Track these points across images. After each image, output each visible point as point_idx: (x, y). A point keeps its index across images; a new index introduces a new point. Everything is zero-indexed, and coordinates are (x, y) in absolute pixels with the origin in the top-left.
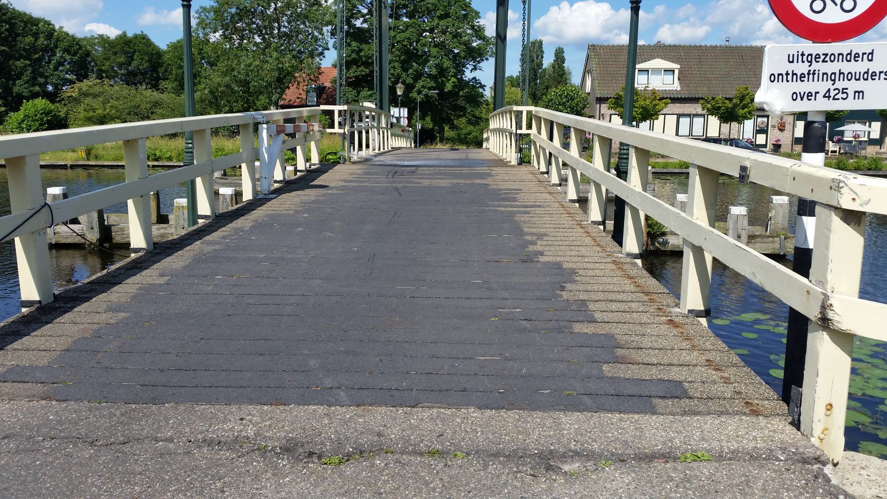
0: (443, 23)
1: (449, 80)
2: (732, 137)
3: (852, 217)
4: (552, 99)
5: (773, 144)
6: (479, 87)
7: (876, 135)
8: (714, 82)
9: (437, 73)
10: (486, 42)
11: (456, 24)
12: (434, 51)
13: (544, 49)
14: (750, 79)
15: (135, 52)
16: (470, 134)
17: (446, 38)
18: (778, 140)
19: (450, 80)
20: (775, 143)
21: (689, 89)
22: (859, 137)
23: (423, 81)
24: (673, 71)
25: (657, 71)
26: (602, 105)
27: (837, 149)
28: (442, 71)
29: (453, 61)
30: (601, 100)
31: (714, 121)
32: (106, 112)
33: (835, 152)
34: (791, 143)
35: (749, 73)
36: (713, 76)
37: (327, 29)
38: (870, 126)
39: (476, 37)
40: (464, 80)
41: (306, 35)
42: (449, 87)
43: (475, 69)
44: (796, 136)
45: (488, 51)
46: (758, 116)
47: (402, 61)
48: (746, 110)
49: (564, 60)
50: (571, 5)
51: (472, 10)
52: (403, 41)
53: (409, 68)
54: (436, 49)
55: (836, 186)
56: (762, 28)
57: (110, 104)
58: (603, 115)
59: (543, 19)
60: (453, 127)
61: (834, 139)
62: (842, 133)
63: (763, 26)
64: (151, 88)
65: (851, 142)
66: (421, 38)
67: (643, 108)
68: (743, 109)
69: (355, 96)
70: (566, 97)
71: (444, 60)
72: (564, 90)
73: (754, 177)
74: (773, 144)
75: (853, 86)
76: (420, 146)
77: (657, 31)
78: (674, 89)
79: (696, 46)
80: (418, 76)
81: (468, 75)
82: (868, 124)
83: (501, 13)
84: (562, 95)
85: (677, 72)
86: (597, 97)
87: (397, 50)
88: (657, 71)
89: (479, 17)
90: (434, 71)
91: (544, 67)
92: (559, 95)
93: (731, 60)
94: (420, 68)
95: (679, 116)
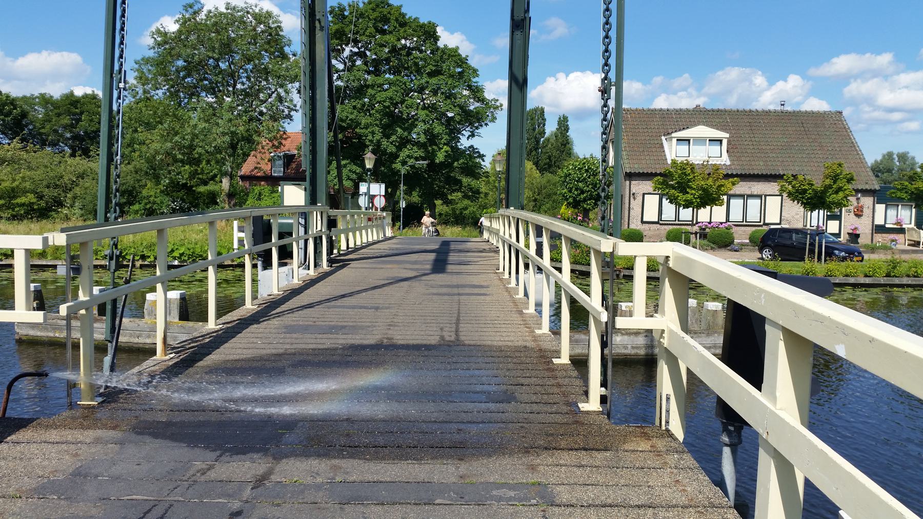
0: (434, 81)
1: (440, 149)
4: (570, 174)
5: (848, 233)
6: (477, 157)
8: (771, 155)
9: (425, 140)
10: (486, 105)
11: (449, 83)
12: (422, 114)
13: (546, 116)
14: (816, 152)
15: (82, 113)
16: (466, 209)
17: (437, 100)
18: (856, 229)
19: (442, 149)
20: (851, 231)
21: (741, 163)
23: (409, 150)
24: (721, 141)
25: (700, 141)
26: (633, 182)
28: (432, 139)
29: (446, 126)
30: (630, 176)
32: (14, 185)
34: (871, 231)
36: (768, 147)
37: (294, 87)
39: (474, 99)
40: (459, 149)
41: (269, 94)
42: (440, 157)
43: (473, 135)
44: (876, 223)
45: (488, 116)
47: (385, 125)
49: (568, 129)
50: (567, 76)
51: (469, 67)
52: (384, 101)
53: (392, 134)
54: (425, 111)
56: (760, 99)
57: (21, 175)
58: (634, 194)
59: (539, 88)
60: (447, 202)
63: (760, 97)
64: (80, 156)
66: (407, 98)
67: (704, 190)
68: (837, 192)
70: (587, 171)
71: (435, 125)
72: (584, 163)
74: (848, 233)
76: (403, 228)
77: (653, 101)
78: (722, 163)
79: (745, 111)
80: (403, 143)
81: (464, 142)
83: (519, 42)
84: (582, 168)
85: (725, 142)
86: (626, 173)
87: (377, 111)
88: (700, 141)
89: (477, 76)
90: (423, 139)
91: (546, 135)
92: (579, 169)
93: (790, 129)
94: (406, 134)
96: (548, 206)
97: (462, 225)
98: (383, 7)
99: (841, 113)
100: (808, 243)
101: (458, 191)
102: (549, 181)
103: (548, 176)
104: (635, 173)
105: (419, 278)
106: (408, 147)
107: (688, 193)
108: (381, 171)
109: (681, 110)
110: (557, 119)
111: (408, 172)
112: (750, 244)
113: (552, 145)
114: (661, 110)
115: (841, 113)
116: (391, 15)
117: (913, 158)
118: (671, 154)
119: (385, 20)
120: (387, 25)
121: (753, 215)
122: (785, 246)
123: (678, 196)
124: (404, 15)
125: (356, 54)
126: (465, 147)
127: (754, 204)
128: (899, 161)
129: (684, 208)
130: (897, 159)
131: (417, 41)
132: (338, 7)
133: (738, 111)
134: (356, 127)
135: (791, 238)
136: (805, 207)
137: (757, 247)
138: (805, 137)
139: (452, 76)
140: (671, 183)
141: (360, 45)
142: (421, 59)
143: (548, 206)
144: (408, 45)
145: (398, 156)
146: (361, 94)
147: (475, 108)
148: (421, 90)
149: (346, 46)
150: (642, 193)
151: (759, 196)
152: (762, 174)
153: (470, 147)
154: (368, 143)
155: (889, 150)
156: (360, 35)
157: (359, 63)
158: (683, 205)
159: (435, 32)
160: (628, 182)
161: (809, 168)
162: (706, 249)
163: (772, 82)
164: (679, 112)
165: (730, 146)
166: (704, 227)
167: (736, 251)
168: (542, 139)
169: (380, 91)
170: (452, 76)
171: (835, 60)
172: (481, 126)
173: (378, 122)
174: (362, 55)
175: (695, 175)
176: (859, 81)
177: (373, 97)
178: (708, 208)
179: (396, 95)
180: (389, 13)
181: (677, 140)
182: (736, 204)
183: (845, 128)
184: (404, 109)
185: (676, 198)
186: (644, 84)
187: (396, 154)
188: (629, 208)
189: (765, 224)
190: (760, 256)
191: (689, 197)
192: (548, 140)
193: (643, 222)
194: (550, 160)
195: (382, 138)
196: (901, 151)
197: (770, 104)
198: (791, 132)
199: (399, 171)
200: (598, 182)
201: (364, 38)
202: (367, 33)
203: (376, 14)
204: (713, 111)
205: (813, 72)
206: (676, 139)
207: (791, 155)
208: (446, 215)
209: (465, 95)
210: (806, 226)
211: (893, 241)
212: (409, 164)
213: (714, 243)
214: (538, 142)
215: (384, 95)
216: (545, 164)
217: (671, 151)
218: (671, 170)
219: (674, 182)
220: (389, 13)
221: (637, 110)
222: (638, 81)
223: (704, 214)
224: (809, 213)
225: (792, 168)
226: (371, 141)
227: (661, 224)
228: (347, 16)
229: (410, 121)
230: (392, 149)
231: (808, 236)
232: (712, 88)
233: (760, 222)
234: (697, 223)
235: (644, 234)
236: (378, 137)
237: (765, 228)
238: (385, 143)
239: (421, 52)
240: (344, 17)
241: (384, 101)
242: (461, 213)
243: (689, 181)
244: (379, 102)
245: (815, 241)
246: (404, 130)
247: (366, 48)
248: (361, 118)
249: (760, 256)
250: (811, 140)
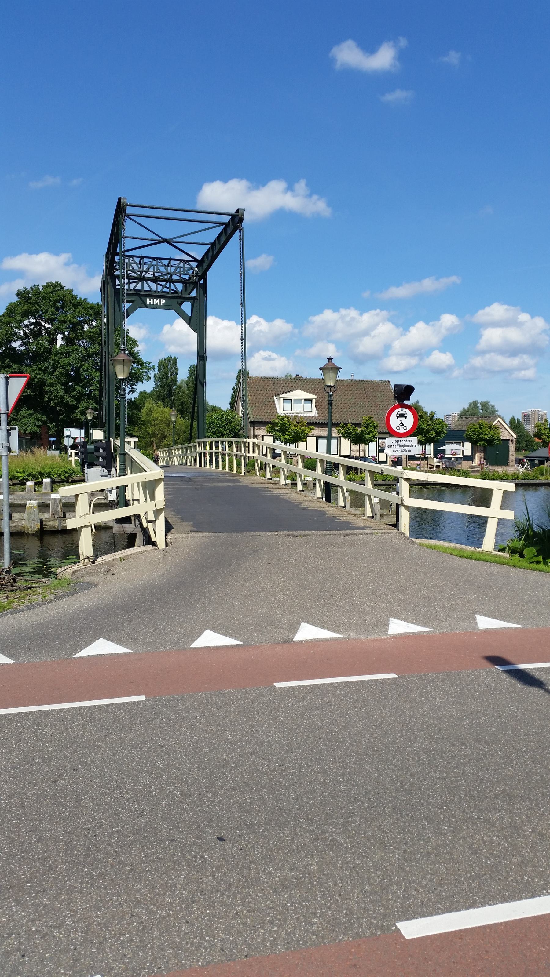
2: (361, 456)
3: (406, 480)
7: (468, 453)
14: (372, 408)
20: (393, 460)
22: (456, 454)
25: (298, 400)
26: (256, 428)
27: (440, 464)
30: (254, 424)
31: (345, 443)
33: (439, 466)
35: (370, 403)
38: (463, 446)
46: (379, 438)
48: (371, 435)
55: (402, 473)
58: (256, 436)
61: (438, 457)
62: (443, 451)
65: (450, 458)
67: (295, 433)
69: (14, 415)
72: (222, 415)
73: (385, 472)
75: (408, 448)
82: (462, 444)
85: (314, 401)
91: (178, 383)
93: (356, 392)
95: (318, 438)
99: (389, 381)
110: (188, 369)
114: (273, 378)
115: (389, 381)
117: (493, 406)
124: (75, 297)
128: (482, 409)
130: (480, 407)
132: (24, 291)
155: (475, 400)
165: (318, 404)
187: (76, 406)
191: (287, 436)
194: (183, 407)
196: (484, 400)
198: (357, 395)
207: (356, 410)
211: (418, 465)
217: (280, 407)
221: (257, 377)
230: (73, 402)
236: (61, 393)
238: (67, 397)
240: (30, 298)
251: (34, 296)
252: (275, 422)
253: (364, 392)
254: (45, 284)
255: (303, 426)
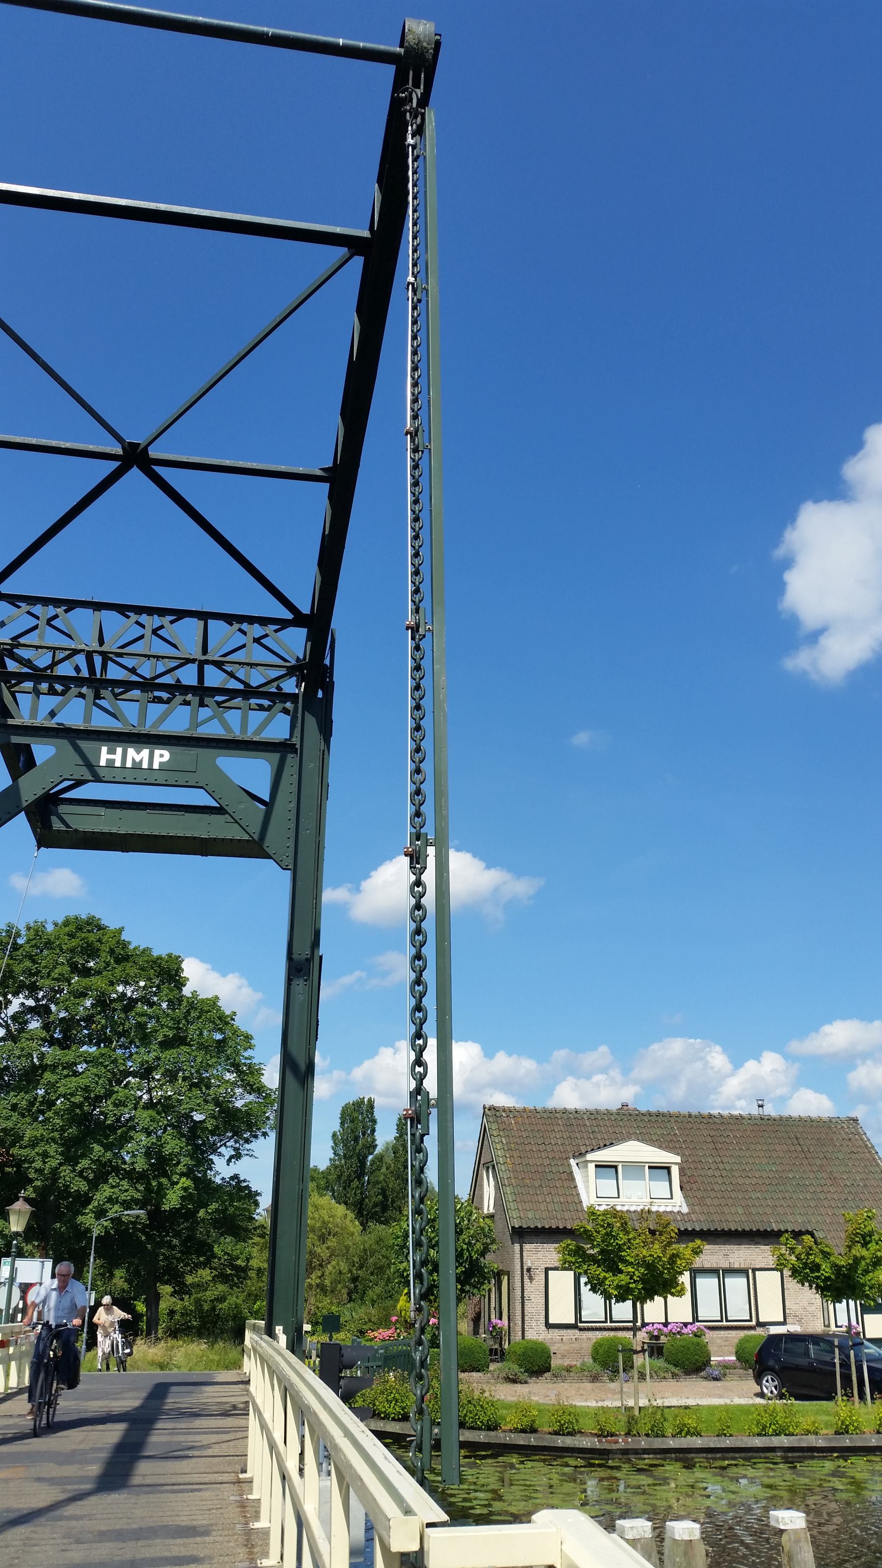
0: (169, 1055)
8: (754, 1195)
10: (265, 1098)
12: (144, 1117)
13: (377, 1114)
14: (825, 1189)
16: (221, 1299)
19: (177, 1183)
25: (634, 1168)
26: (527, 1247)
30: (522, 1234)
35: (819, 1175)
36: (747, 1181)
42: (172, 1199)
43: (237, 1156)
47: (70, 1139)
52: (72, 1095)
53: (83, 1156)
60: (181, 1290)
67: (650, 1266)
78: (676, 1210)
85: (675, 1171)
86: (513, 1228)
90: (141, 1164)
93: (778, 1147)
94: (109, 1155)
96: (378, 1290)
97: (208, 1337)
98: (89, 931)
100: (837, 1361)
101: (205, 1267)
102: (379, 1241)
103: (378, 1229)
104: (529, 1228)
105: (58, 1513)
106: (111, 1181)
107: (621, 1272)
108: (55, 1229)
109: (598, 1112)
111: (107, 1232)
112: (738, 1364)
113: (387, 1169)
114: (565, 1111)
116: (102, 943)
118: (588, 1192)
119: (91, 951)
120: (93, 960)
121: (738, 1310)
122: (797, 1368)
123: (605, 1278)
124: (125, 945)
125: (31, 1010)
126: (223, 1179)
127: (736, 1285)
129: (617, 1301)
131: (144, 988)
133: (690, 1116)
134: (13, 1145)
135: (807, 1353)
136: (823, 1296)
137: (751, 1371)
138: (805, 1162)
139: (203, 1047)
140: (591, 1252)
141: (41, 994)
142: (150, 1018)
143: (378, 1290)
144: (129, 994)
145: (88, 1200)
146: (29, 1082)
147: (245, 1105)
148: (146, 1073)
149: (14, 995)
150: (543, 1267)
151: (742, 1272)
152: (744, 1230)
153: (232, 1178)
154: (32, 1175)
156: (42, 977)
157: (34, 1025)
158: (615, 1296)
159: (179, 969)
160: (517, 1247)
161: (819, 1218)
162: (664, 1378)
163: (737, 1063)
164: (595, 1115)
165: (685, 1179)
166: (656, 1333)
167: (716, 1379)
168: (370, 1157)
169: (66, 1076)
170: (203, 1047)
171: (827, 1029)
172: (256, 1137)
173: (56, 1135)
174: (41, 1011)
175: (631, 1236)
176: (869, 1062)
177: (51, 1086)
178: (658, 1300)
179: (97, 1083)
180: (99, 940)
181: (597, 1166)
182: (707, 1286)
183: (866, 1146)
184: (110, 1108)
185: (601, 1283)
186: (540, 1062)
187: (86, 1194)
188: (523, 1297)
189: (760, 1324)
190: (757, 1389)
191: (623, 1279)
192: (380, 1158)
193: (549, 1326)
195: (61, 1164)
197: (739, 1098)
198: (781, 1154)
199: (88, 1230)
200: (465, 1247)
201: (48, 982)
202: (55, 975)
203: (74, 942)
204: (650, 1114)
205: (795, 1046)
206: (594, 1164)
208: (182, 1315)
209: (228, 1081)
210: (829, 1326)
212: (111, 1214)
213: (676, 1366)
214: (363, 1162)
215: (73, 1082)
216: (375, 1205)
217: (587, 1187)
218: (589, 1228)
219: (596, 1250)
220: (99, 940)
222: (530, 1057)
223: (653, 1310)
224: (831, 1307)
225: (791, 1218)
226: (39, 1171)
227: (581, 1329)
228: (21, 946)
229: (119, 1131)
231: (837, 1350)
232: (645, 1072)
233: (751, 1320)
234: (644, 1325)
235: (553, 1349)
237: (760, 1331)
238: (66, 1172)
239: (151, 1004)
241: (72, 1095)
242: (213, 1309)
243: (620, 1248)
244: (64, 1096)
245: (848, 1357)
246: (107, 1147)
247: (52, 1000)
248: (25, 1126)
249: (757, 1389)
250: (815, 1169)
251: (28, 941)
252: (586, 1231)
253: (799, 1148)
254: (60, 920)
255: (669, 1244)
